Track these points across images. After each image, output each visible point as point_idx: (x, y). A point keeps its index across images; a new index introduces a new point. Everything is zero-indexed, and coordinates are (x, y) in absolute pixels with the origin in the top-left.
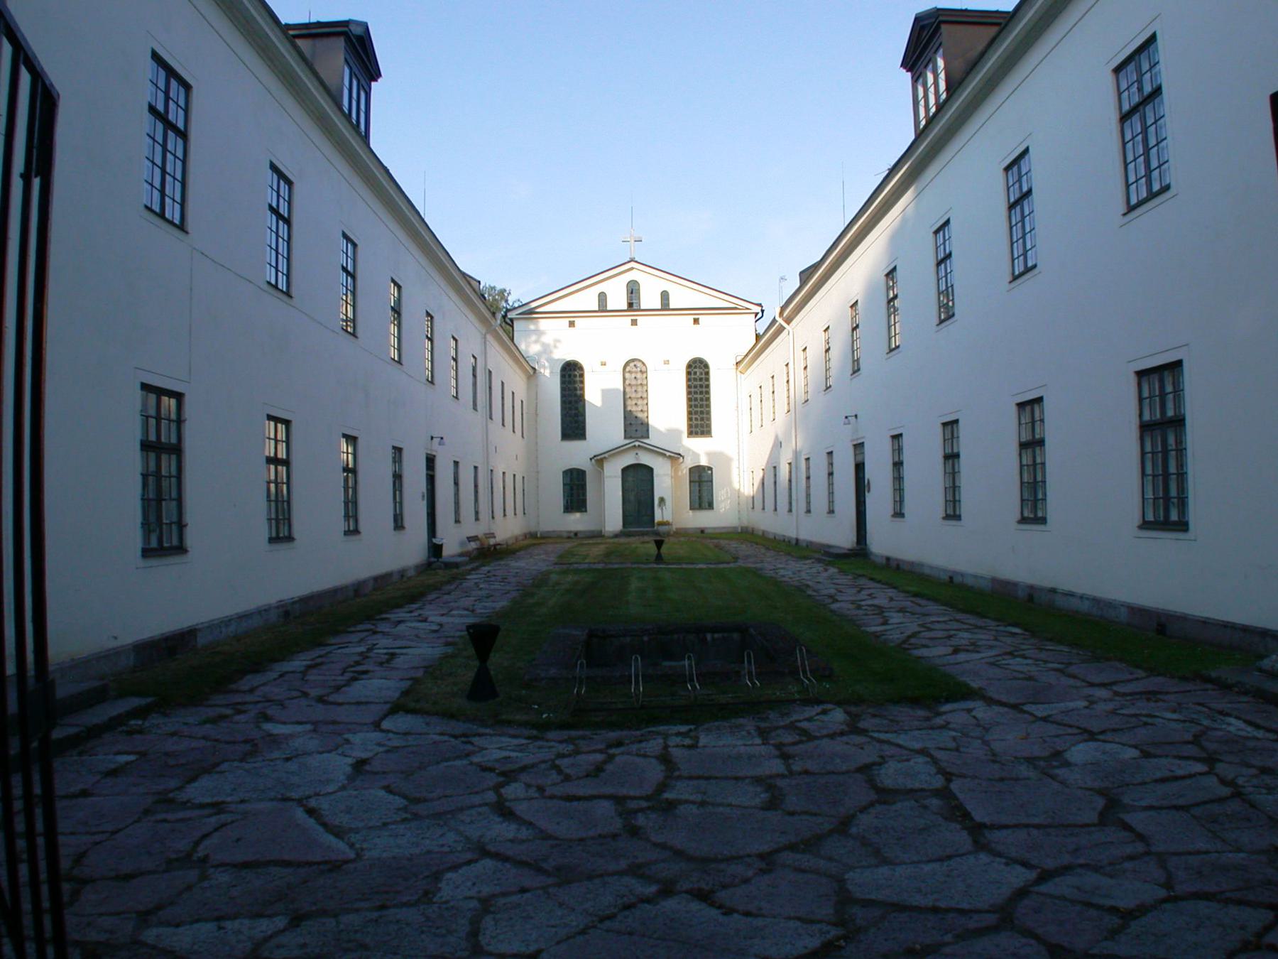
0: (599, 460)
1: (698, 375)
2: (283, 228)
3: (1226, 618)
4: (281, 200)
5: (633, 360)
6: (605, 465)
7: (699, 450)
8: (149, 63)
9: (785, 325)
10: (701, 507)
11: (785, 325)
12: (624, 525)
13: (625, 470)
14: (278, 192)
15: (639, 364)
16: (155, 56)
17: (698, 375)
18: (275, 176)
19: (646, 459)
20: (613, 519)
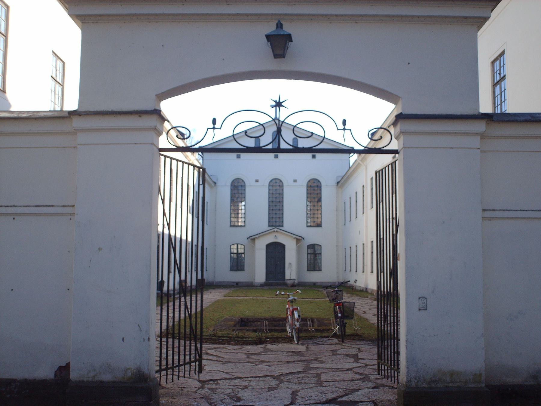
0: (253, 239)
1: (314, 189)
2: (59, 88)
3: (86, 110)
4: (58, 72)
5: (276, 179)
6: (257, 242)
7: (313, 236)
8: (52, 53)
9: (360, 162)
10: (314, 270)
11: (360, 162)
12: (267, 279)
13: (268, 246)
14: (56, 68)
15: (277, 181)
16: (53, 52)
17: (314, 189)
18: (55, 58)
19: (281, 239)
20: (260, 274)
